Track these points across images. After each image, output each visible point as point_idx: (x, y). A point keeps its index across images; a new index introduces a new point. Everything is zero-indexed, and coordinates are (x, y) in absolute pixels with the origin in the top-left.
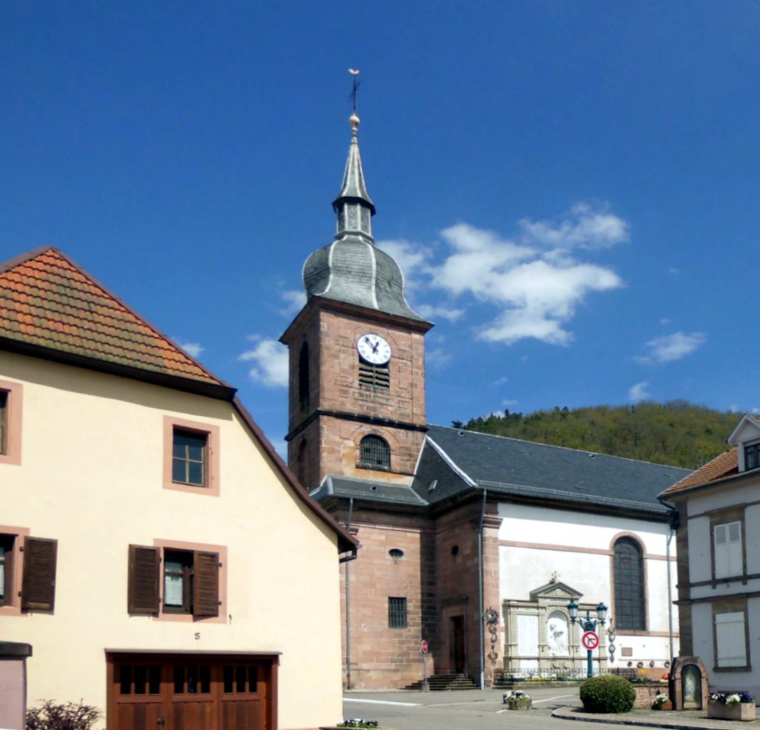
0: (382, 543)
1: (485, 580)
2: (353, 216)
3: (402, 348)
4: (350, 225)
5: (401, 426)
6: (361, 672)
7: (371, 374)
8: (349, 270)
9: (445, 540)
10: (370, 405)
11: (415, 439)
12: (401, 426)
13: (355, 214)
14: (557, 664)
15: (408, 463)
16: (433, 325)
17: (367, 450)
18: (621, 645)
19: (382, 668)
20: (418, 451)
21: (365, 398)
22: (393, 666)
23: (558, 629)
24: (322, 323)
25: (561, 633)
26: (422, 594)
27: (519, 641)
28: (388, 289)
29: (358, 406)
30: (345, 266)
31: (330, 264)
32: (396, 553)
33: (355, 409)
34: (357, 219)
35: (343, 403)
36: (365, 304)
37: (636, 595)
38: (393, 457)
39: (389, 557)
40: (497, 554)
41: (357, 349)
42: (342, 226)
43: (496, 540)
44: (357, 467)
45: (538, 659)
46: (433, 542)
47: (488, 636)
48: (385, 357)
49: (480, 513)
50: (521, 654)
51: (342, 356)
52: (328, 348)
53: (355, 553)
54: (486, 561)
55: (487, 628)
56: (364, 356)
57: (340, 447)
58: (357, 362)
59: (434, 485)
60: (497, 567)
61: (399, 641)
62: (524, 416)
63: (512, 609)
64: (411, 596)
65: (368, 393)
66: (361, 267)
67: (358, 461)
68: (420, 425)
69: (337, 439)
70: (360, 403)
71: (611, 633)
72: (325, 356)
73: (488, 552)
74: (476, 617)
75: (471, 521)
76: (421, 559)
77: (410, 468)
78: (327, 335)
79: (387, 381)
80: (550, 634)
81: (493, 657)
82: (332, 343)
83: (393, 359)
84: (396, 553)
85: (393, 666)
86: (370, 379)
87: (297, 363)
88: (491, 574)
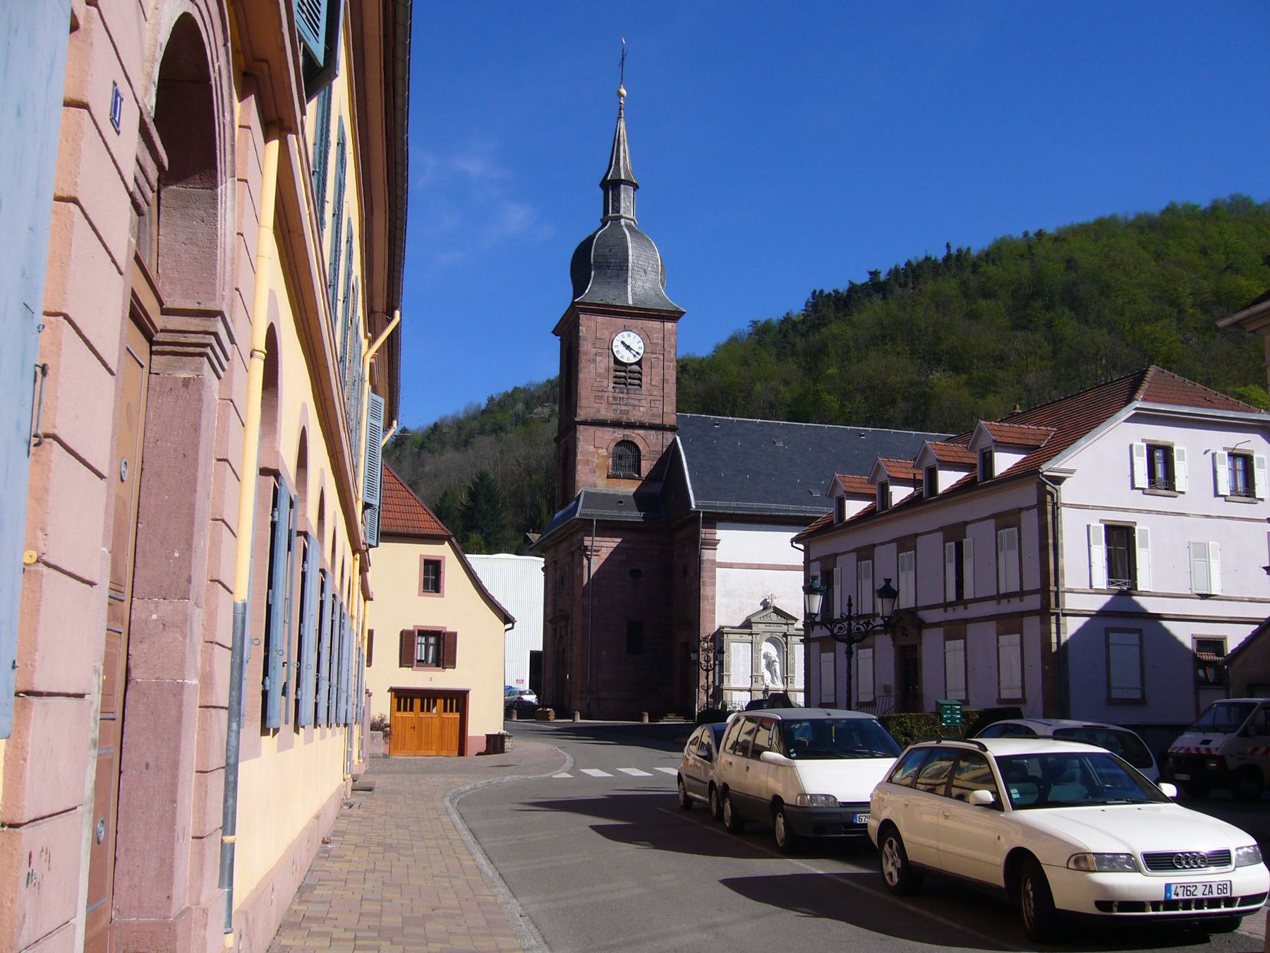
3: (655, 341)
5: (652, 427)
10: (623, 408)
12: (652, 427)
16: (685, 313)
17: (620, 457)
21: (618, 402)
24: (581, 328)
30: (604, 260)
33: (609, 414)
43: (714, 562)
49: (698, 533)
50: (733, 685)
53: (513, 624)
56: (619, 357)
62: (974, 253)
65: (621, 396)
69: (591, 448)
70: (614, 407)
73: (705, 575)
78: (585, 339)
82: (590, 346)
88: (708, 599)
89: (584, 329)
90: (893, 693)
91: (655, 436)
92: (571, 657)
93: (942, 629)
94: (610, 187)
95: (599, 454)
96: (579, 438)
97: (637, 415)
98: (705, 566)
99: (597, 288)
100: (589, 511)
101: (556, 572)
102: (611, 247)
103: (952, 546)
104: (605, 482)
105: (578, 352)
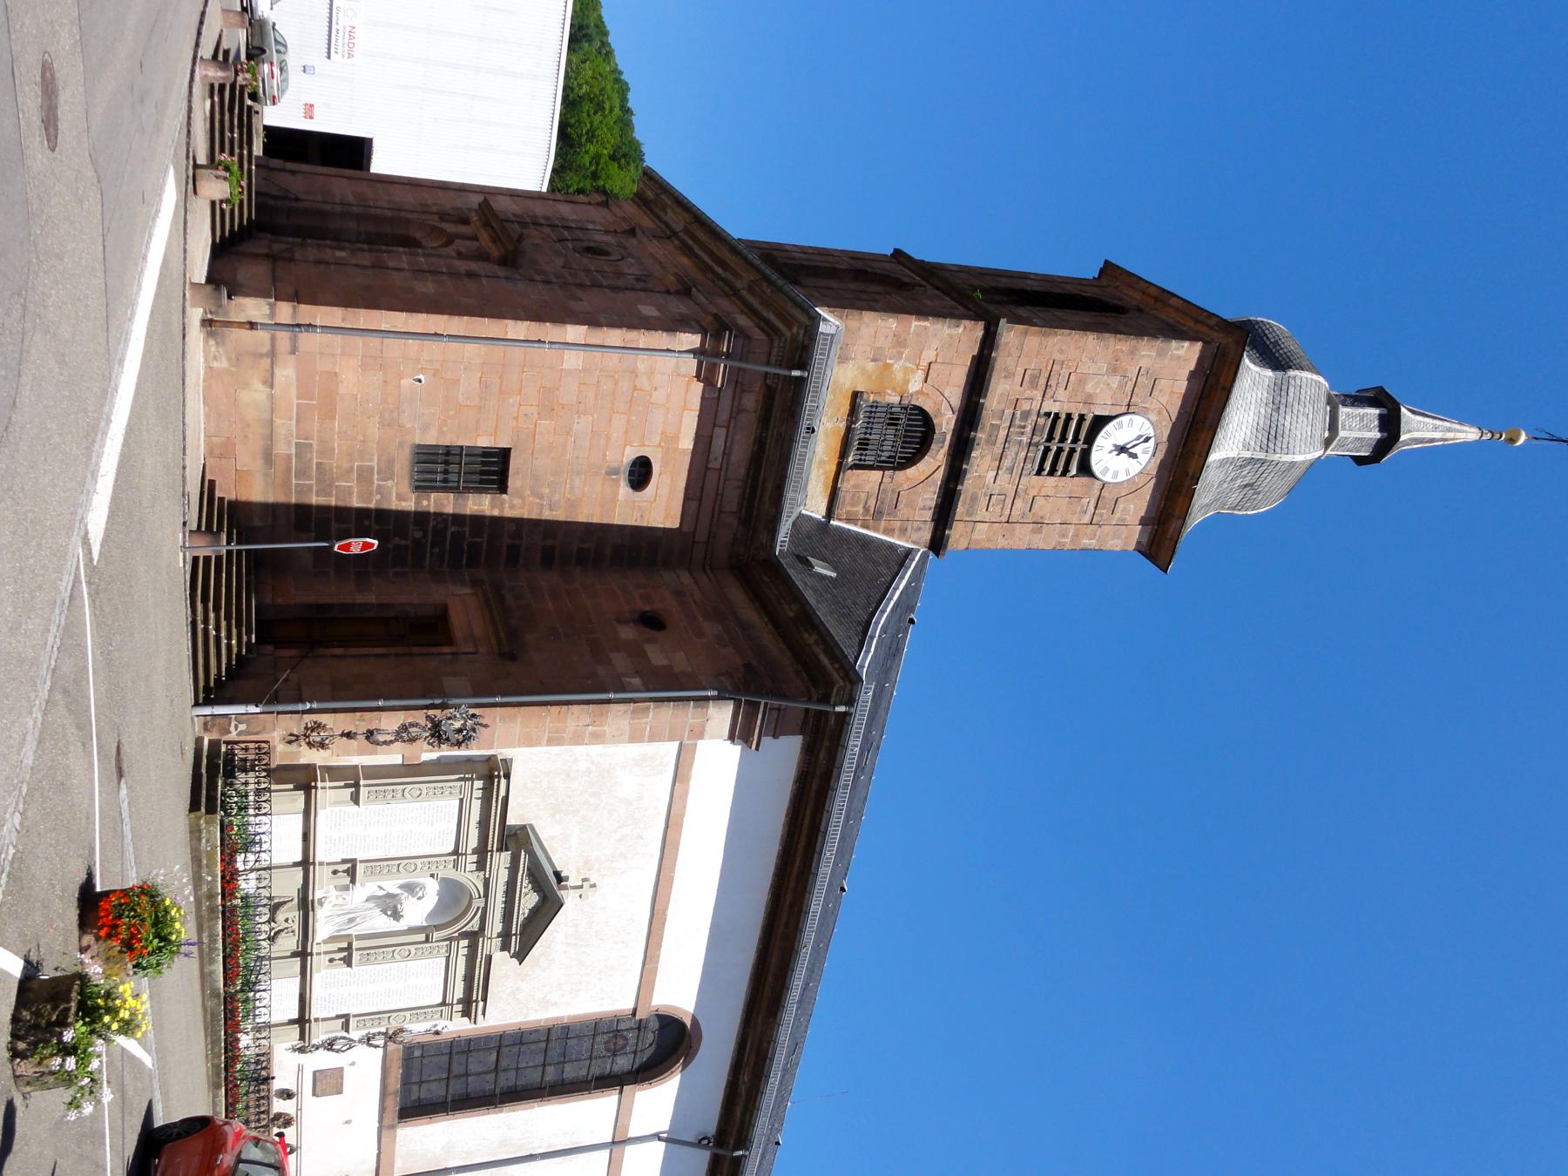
0: (670, 439)
1: (575, 708)
3: (1121, 506)
4: (1348, 415)
6: (266, 362)
8: (1282, 408)
9: (679, 594)
10: (1003, 433)
11: (916, 525)
14: (289, 916)
15: (860, 509)
17: (893, 421)
18: (353, 1064)
19: (278, 421)
20: (888, 531)
21: (1017, 422)
22: (284, 448)
24: (1186, 344)
27: (367, 809)
28: (1238, 482)
29: (1002, 406)
31: (1291, 373)
32: (640, 473)
35: (1009, 375)
36: (1220, 435)
37: (507, 1080)
38: (877, 475)
39: (630, 454)
40: (654, 738)
43: (699, 733)
44: (856, 396)
45: (306, 863)
47: (390, 722)
52: (1133, 352)
55: (419, 717)
56: (1110, 427)
57: (908, 359)
59: (821, 569)
60: (615, 739)
61: (371, 468)
63: (479, 784)
65: (1029, 429)
66: (1287, 432)
68: (949, 536)
69: (929, 355)
70: (1009, 412)
71: (390, 1037)
72: (1118, 345)
73: (666, 715)
74: (449, 682)
75: (748, 666)
76: (622, 528)
77: (848, 513)
78: (1161, 354)
79: (1064, 473)
81: (315, 737)
83: (1098, 485)
84: (640, 473)
85: (284, 448)
86: (1057, 435)
87: (1071, 289)
89: (1181, 352)
95: (913, 371)
97: (980, 465)
98: (688, 715)
104: (847, 385)
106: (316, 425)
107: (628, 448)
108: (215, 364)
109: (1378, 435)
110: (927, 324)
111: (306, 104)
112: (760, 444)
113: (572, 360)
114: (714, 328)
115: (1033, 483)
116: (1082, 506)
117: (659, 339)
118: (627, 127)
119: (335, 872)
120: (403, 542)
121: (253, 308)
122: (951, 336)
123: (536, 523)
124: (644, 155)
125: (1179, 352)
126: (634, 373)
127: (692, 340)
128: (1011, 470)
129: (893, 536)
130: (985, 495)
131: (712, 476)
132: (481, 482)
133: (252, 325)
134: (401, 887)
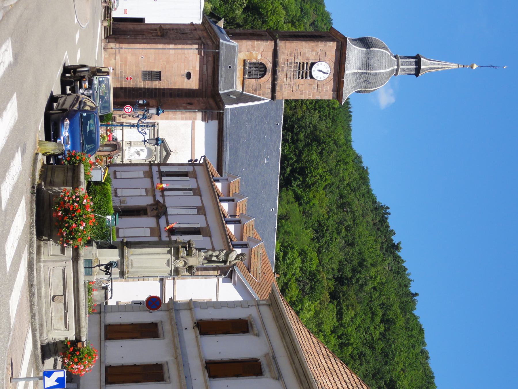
0: (194, 68)
2: (409, 63)
3: (325, 87)
6: (114, 55)
7: (305, 69)
8: (370, 59)
10: (285, 68)
11: (266, 93)
13: (410, 65)
19: (117, 67)
21: (289, 65)
22: (118, 72)
23: (141, 153)
24: (332, 42)
25: (139, 155)
26: (164, 89)
28: (362, 80)
29: (284, 61)
31: (372, 49)
32: (189, 76)
34: (408, 65)
35: (284, 53)
40: (186, 119)
41: (320, 61)
42: (402, 58)
43: (195, 119)
46: (197, 97)
48: (317, 77)
51: (314, 53)
52: (317, 46)
54: (182, 113)
56: (315, 65)
58: (311, 61)
64: (162, 84)
65: (293, 67)
66: (372, 64)
67: (249, 61)
70: (286, 63)
73: (188, 114)
79: (302, 78)
80: (139, 148)
81: (124, 116)
83: (316, 81)
84: (189, 76)
86: (301, 69)
88: (174, 116)
90: (122, 205)
91: (269, 87)
92: (139, 39)
93: (156, 226)
94: (417, 60)
95: (258, 54)
96: (267, 42)
97: (281, 77)
98: (193, 115)
99: (359, 51)
100: (224, 48)
101: (190, 30)
102: (380, 60)
103: (186, 169)
105: (318, 41)
106: (124, 67)
107: (185, 70)
108: (106, 56)
109: (415, 67)
110: (259, 42)
111: (125, 10)
112: (214, 68)
113: (172, 52)
114: (200, 44)
115: (297, 81)
116: (313, 87)
117: (189, 46)
118: (320, 5)
119: (128, 143)
120: (141, 92)
121: (112, 45)
122: (266, 45)
123: (167, 89)
124: (331, 21)
125: (330, 45)
126: (185, 54)
127: (196, 46)
128: (290, 78)
129: (261, 96)
130: (284, 85)
131: (204, 76)
132: (156, 79)
133: (112, 48)
134: (140, 150)
